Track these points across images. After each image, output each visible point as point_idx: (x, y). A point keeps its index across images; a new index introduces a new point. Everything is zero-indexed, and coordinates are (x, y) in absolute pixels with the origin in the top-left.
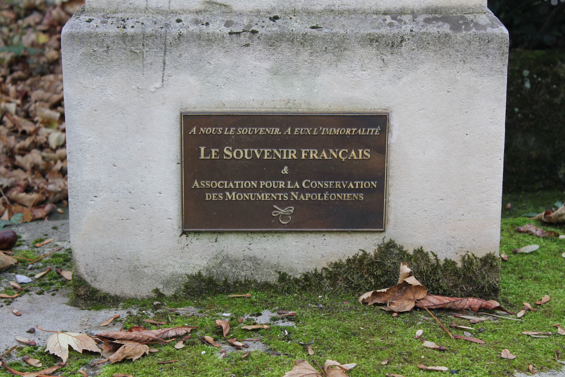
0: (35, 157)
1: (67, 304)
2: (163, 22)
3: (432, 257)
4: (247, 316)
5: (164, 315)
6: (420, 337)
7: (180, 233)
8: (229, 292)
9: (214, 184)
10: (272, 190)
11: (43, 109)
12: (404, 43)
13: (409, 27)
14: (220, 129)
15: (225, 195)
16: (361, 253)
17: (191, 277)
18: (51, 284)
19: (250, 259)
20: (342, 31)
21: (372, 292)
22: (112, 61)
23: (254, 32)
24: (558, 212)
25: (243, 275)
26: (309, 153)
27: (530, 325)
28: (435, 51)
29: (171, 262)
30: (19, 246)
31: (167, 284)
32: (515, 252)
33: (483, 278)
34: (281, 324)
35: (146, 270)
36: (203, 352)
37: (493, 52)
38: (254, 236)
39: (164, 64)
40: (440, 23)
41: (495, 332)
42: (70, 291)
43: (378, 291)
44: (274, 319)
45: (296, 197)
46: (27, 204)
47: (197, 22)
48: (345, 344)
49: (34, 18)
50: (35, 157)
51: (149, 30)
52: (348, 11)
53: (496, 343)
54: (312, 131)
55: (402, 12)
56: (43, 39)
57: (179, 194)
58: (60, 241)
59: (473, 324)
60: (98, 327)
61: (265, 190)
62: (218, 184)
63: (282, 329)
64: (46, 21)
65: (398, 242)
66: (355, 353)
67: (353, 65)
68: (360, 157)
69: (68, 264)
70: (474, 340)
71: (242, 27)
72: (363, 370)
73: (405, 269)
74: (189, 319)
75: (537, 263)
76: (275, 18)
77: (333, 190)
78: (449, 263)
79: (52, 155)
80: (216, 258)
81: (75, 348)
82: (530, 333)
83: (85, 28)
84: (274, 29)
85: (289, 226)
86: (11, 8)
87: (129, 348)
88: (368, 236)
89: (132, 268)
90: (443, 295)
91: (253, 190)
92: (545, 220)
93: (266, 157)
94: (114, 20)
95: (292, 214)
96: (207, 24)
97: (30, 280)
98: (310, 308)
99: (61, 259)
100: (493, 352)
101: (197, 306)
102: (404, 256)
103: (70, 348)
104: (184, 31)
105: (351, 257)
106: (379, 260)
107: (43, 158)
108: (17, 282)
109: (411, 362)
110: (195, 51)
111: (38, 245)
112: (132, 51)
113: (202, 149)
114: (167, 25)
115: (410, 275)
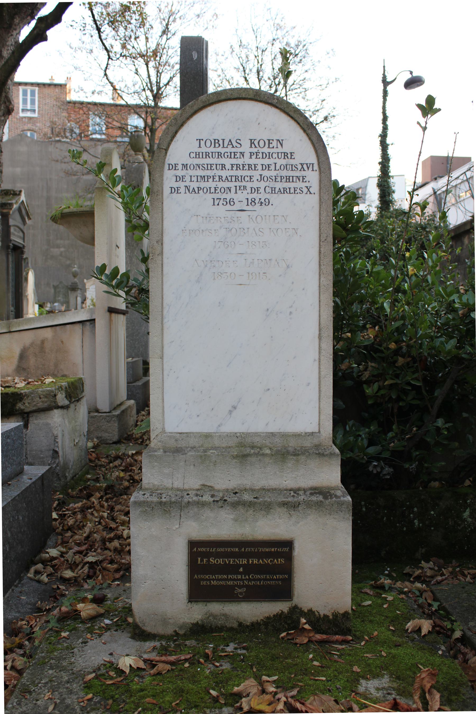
0: (116, 543)
1: (129, 637)
2: (180, 495)
3: (317, 613)
4: (222, 647)
5: (179, 645)
6: (311, 659)
7: (187, 601)
8: (212, 632)
9: (205, 577)
10: (234, 580)
11: (121, 516)
12: (300, 506)
13: (303, 497)
14: (208, 549)
15: (210, 582)
16: (280, 612)
17: (193, 624)
18: (122, 625)
19: (223, 615)
20: (269, 500)
21: (286, 633)
22: (154, 515)
23: (225, 500)
24: (381, 581)
25: (220, 623)
26: (253, 561)
27: (368, 650)
28: (316, 509)
29: (183, 616)
30: (106, 601)
31: (181, 628)
32: (360, 605)
33: (343, 624)
34: (239, 652)
35: (170, 620)
36: (199, 669)
37: (344, 509)
38: (226, 603)
39: (181, 516)
40: (318, 495)
41: (349, 655)
42: (131, 630)
43: (290, 632)
44: (236, 649)
45: (247, 583)
46: (111, 570)
47: (197, 495)
48: (272, 664)
49: (117, 462)
50: (116, 543)
51: (173, 500)
52: (272, 489)
53: (351, 662)
54: (255, 550)
55: (299, 489)
56: (122, 474)
57: (187, 581)
58: (127, 598)
59: (338, 650)
60: (145, 652)
61: (231, 580)
62: (207, 577)
63: (240, 655)
64: (124, 464)
65: (300, 606)
66: (277, 669)
67: (275, 516)
68: (279, 563)
69: (131, 613)
70: (339, 660)
71: (219, 498)
72: (282, 680)
73: (303, 621)
74: (192, 649)
75: (371, 612)
76: (236, 493)
77: (266, 580)
78: (326, 616)
79: (124, 542)
80: (206, 614)
81: (133, 666)
82: (368, 655)
83: (142, 498)
84: (235, 499)
85: (243, 598)
86: (107, 457)
87: (161, 666)
88: (284, 603)
89: (163, 619)
90: (322, 633)
91: (225, 580)
92: (374, 585)
93: (231, 563)
94: (156, 494)
95: (245, 592)
96: (202, 496)
97: (111, 623)
98: (254, 641)
99: (127, 610)
100: (349, 667)
101: (196, 640)
102: (302, 613)
103: (130, 666)
104: (190, 500)
105: (275, 614)
106: (289, 615)
107: (120, 544)
108: (104, 624)
109: (306, 675)
110: (196, 510)
111: (115, 601)
112: (164, 510)
113: (199, 559)
114: (182, 497)
115: (306, 623)
